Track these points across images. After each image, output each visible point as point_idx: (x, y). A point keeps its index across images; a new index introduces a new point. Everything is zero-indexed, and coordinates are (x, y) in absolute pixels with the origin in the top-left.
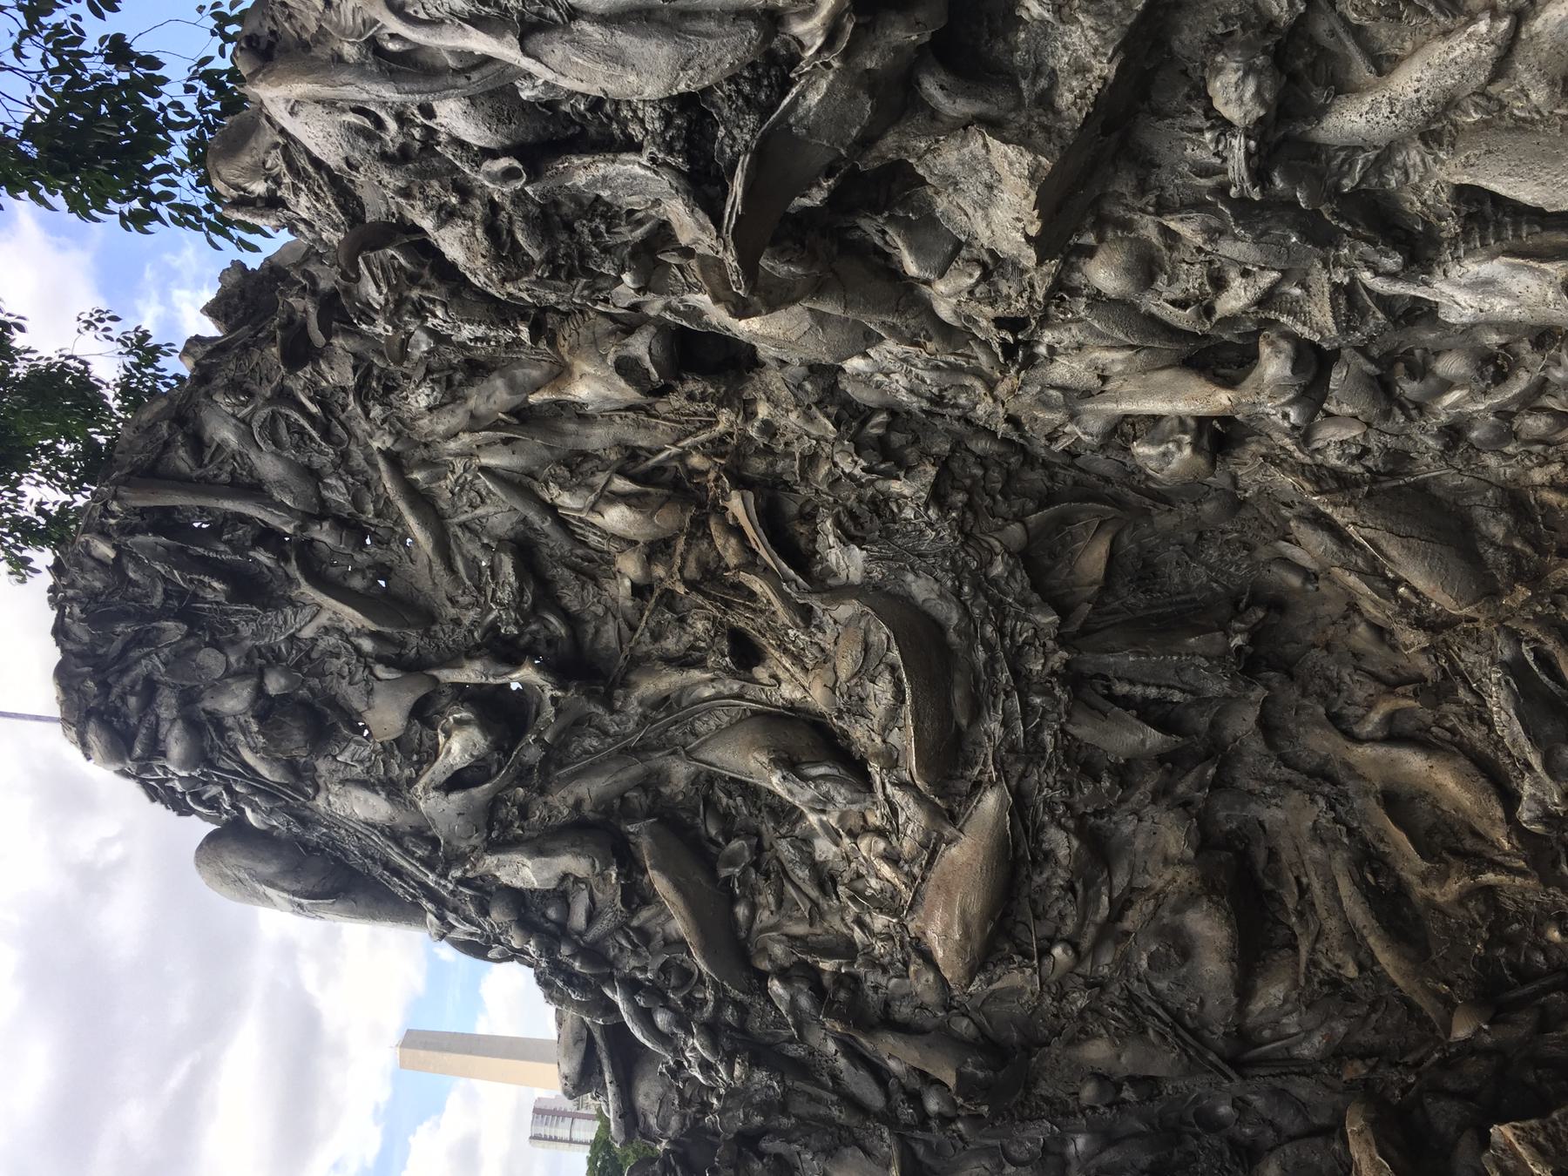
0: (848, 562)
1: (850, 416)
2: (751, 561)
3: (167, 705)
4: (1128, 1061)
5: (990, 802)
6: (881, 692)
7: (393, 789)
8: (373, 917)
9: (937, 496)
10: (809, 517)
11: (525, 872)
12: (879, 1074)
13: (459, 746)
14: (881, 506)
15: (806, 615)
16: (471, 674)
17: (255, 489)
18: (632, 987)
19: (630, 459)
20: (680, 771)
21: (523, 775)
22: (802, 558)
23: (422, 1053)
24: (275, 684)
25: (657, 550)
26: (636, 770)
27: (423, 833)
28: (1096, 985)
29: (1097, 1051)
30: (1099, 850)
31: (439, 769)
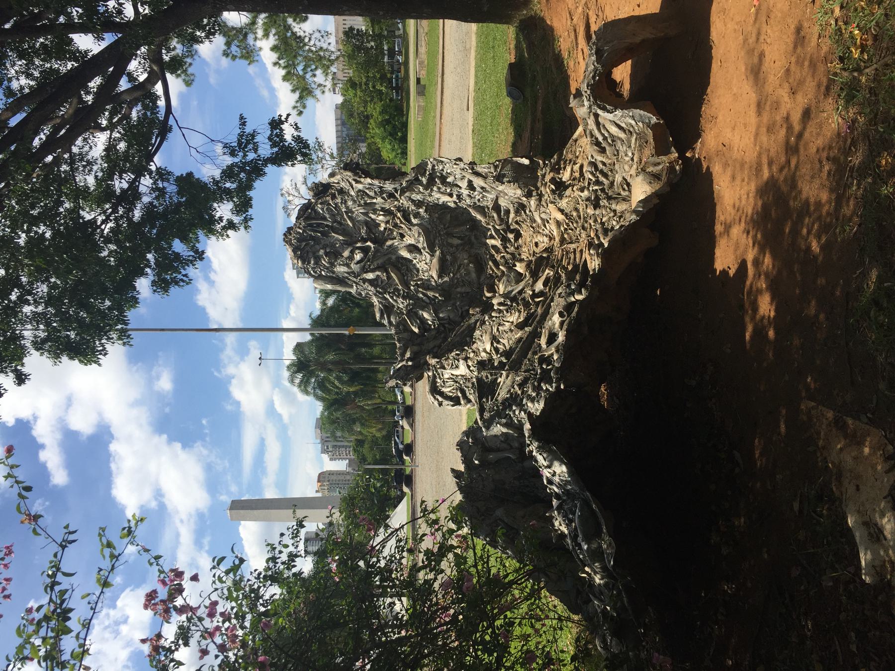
0: (415, 221)
1: (413, 201)
2: (401, 222)
3: (311, 255)
4: (463, 290)
6: (421, 239)
7: (348, 265)
9: (426, 211)
10: (409, 215)
11: (370, 276)
13: (358, 256)
14: (418, 213)
15: (410, 229)
16: (359, 245)
17: (325, 219)
18: (389, 293)
19: (383, 209)
20: (394, 257)
22: (409, 221)
23: (242, 511)
25: (387, 222)
26: (386, 257)
27: (353, 272)
28: (457, 278)
29: (459, 290)
30: (455, 259)
31: (355, 261)
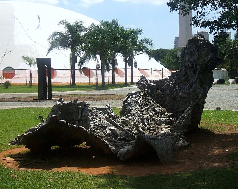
5: (187, 96)
8: (79, 167)
12: (174, 92)
20: (190, 78)
21: (189, 69)
24: (193, 52)
28: (179, 103)
31: (189, 63)
